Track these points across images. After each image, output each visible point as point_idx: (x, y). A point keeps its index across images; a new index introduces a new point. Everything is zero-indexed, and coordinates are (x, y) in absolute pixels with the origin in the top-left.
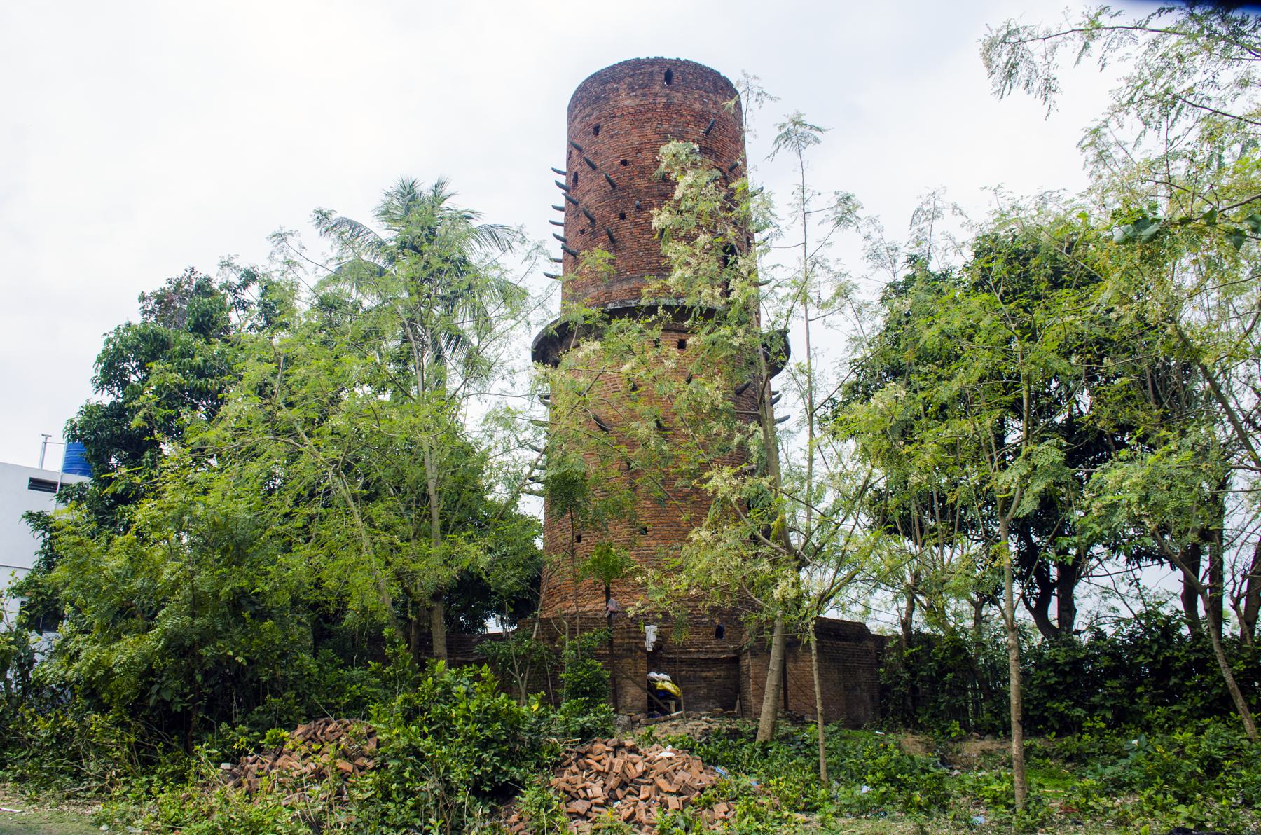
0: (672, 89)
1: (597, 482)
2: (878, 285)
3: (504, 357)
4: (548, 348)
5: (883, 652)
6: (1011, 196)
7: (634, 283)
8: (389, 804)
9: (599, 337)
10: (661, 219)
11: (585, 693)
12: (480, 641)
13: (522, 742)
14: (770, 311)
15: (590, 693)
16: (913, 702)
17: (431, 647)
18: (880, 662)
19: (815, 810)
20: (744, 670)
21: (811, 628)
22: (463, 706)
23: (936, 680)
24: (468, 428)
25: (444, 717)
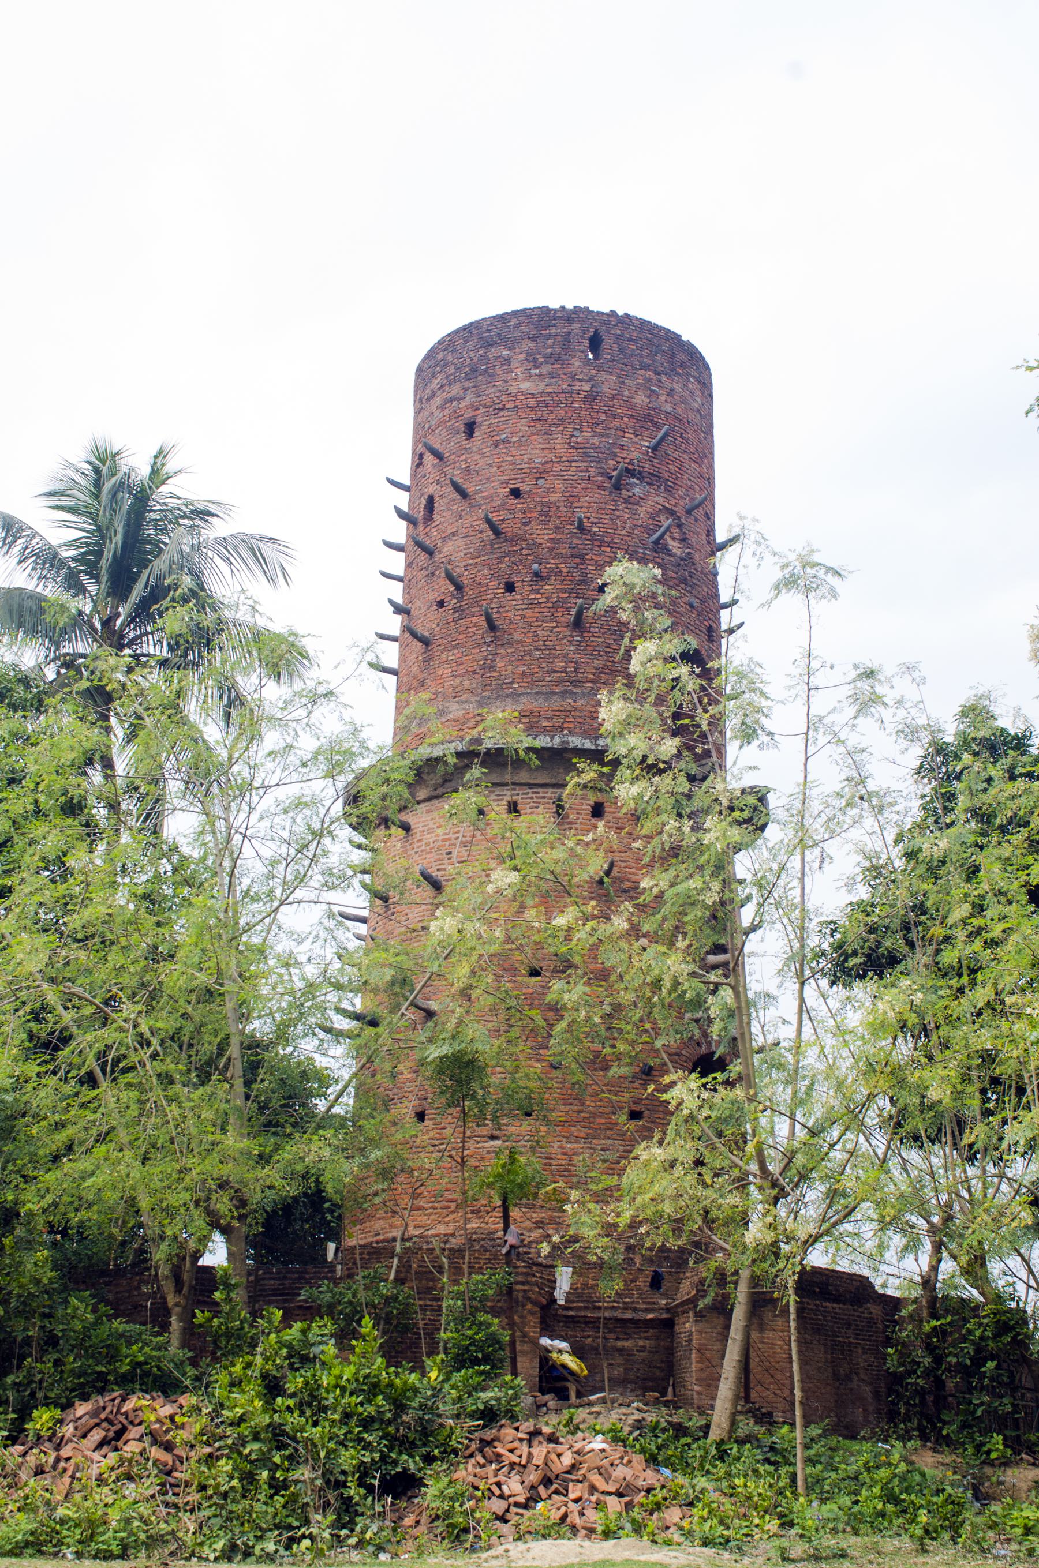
0: (599, 368)
16: (936, 1402)
18: (888, 1339)
21: (790, 1284)
23: (970, 1371)
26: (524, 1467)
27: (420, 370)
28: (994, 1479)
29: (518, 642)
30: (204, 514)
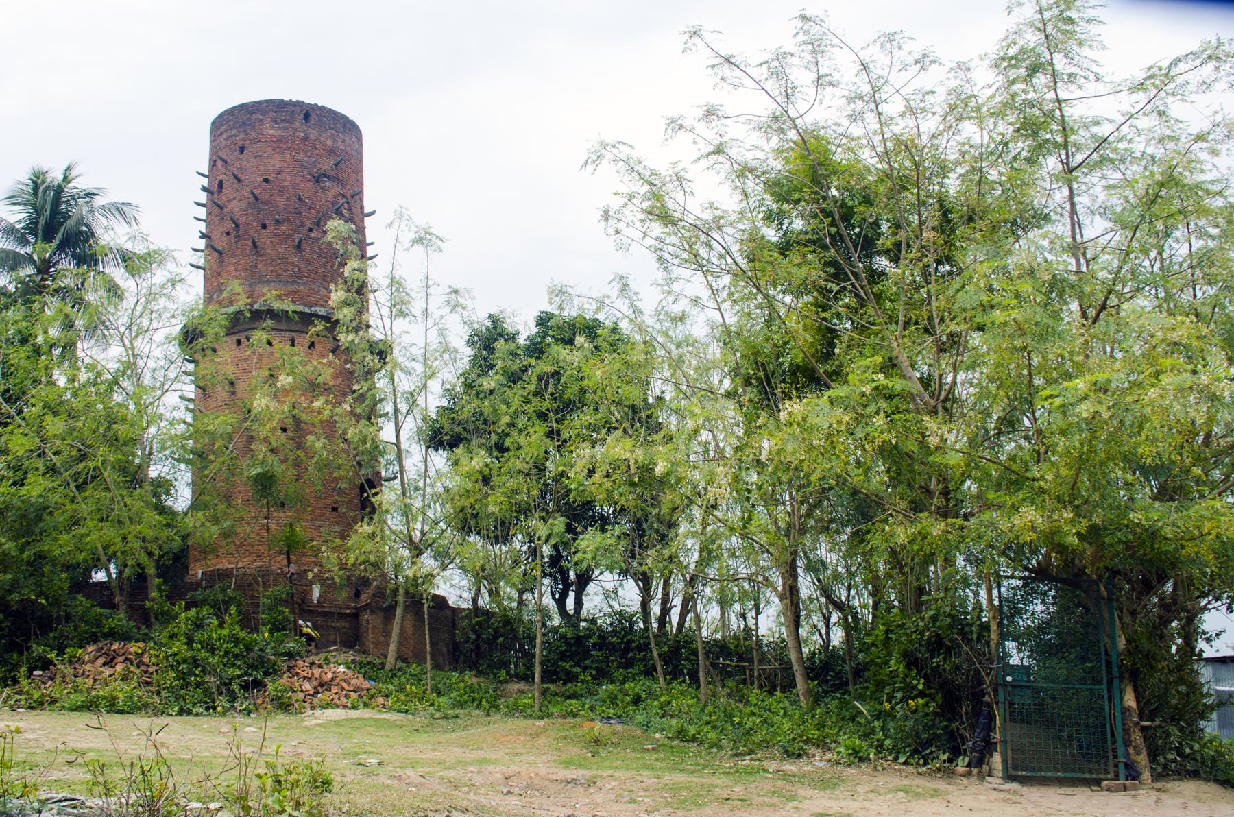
20: (364, 623)
27: (214, 123)
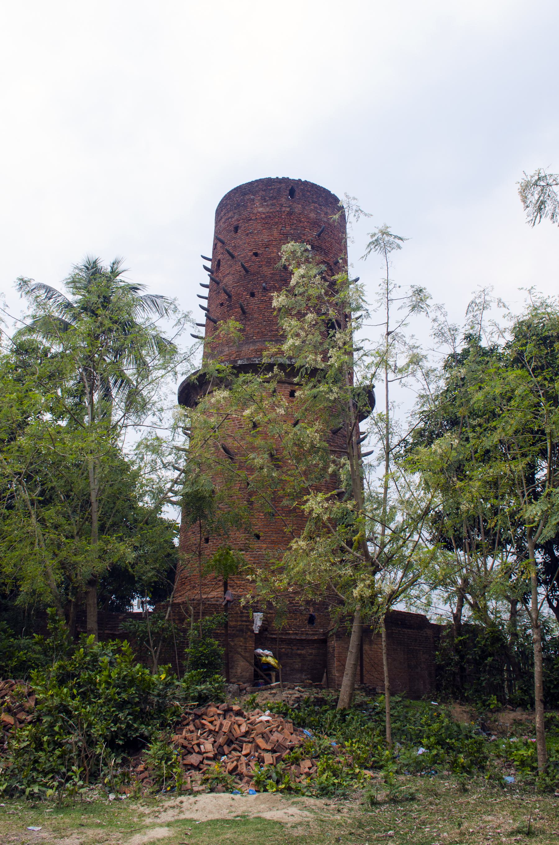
1: (221, 500)
2: (442, 356)
3: (155, 398)
4: (189, 394)
5: (439, 639)
6: (541, 295)
7: (258, 346)
8: (40, 753)
9: (228, 386)
10: (279, 300)
11: (204, 666)
12: (124, 620)
13: (151, 704)
14: (358, 374)
15: (208, 665)
17: (85, 622)
19: (381, 768)
20: (331, 650)
21: (381, 620)
22: (106, 673)
24: (125, 451)
25: (91, 681)
26: (217, 732)
28: (493, 719)
29: (256, 318)
30: (134, 289)
